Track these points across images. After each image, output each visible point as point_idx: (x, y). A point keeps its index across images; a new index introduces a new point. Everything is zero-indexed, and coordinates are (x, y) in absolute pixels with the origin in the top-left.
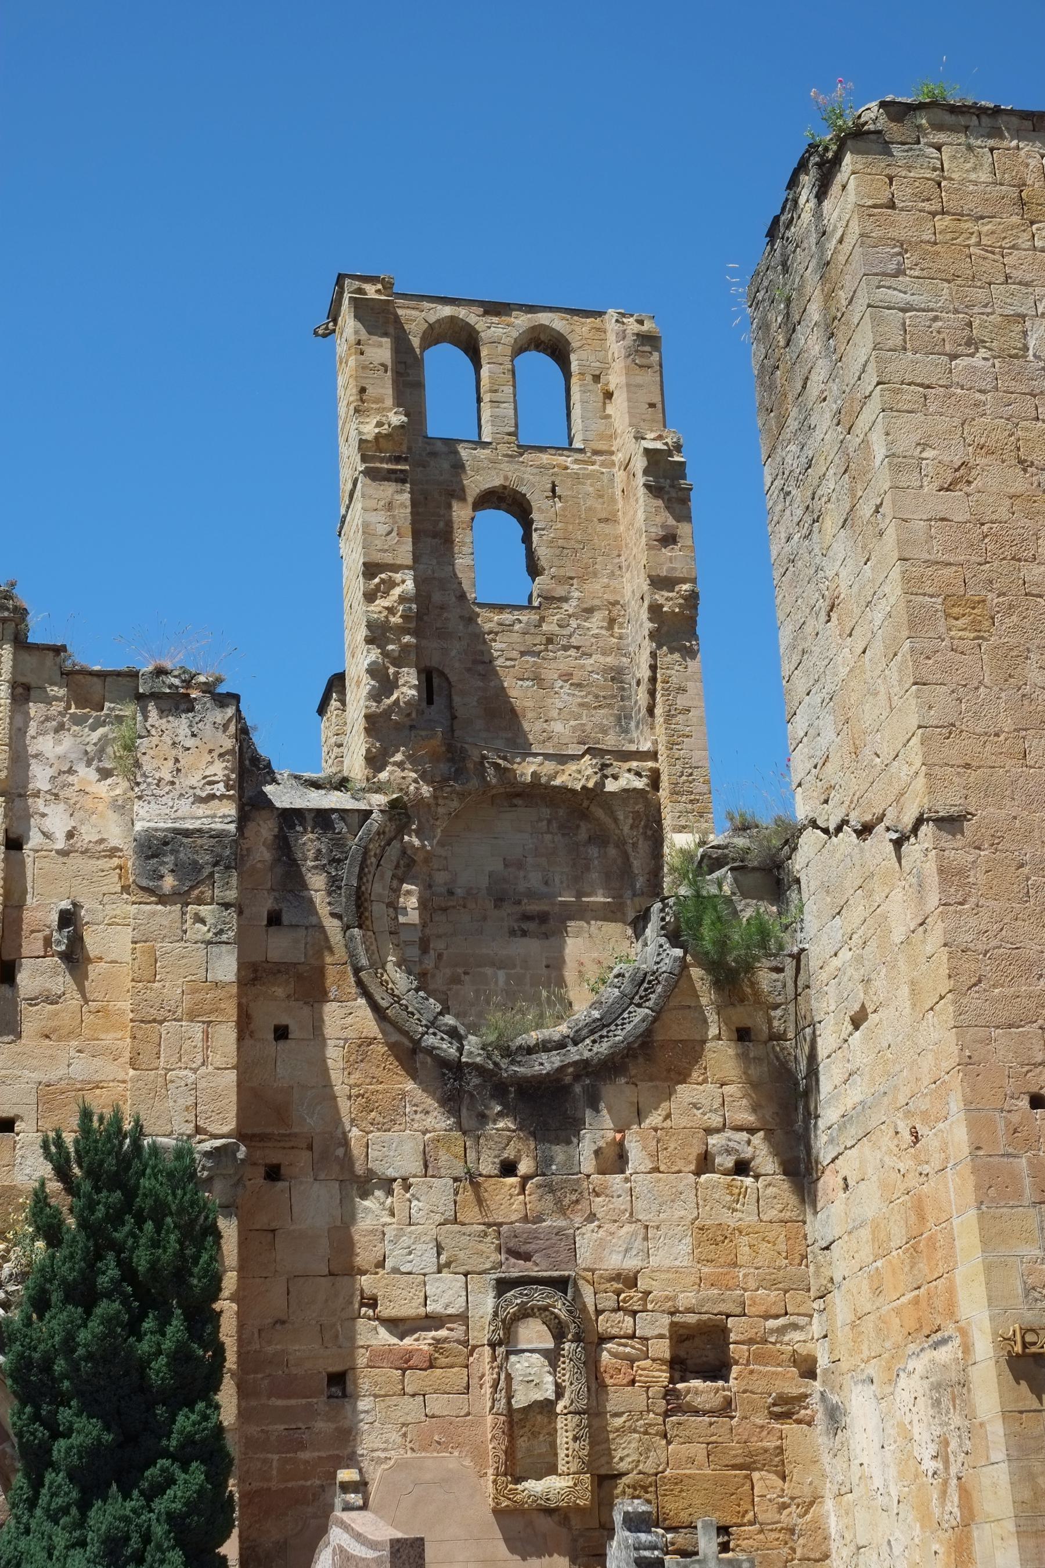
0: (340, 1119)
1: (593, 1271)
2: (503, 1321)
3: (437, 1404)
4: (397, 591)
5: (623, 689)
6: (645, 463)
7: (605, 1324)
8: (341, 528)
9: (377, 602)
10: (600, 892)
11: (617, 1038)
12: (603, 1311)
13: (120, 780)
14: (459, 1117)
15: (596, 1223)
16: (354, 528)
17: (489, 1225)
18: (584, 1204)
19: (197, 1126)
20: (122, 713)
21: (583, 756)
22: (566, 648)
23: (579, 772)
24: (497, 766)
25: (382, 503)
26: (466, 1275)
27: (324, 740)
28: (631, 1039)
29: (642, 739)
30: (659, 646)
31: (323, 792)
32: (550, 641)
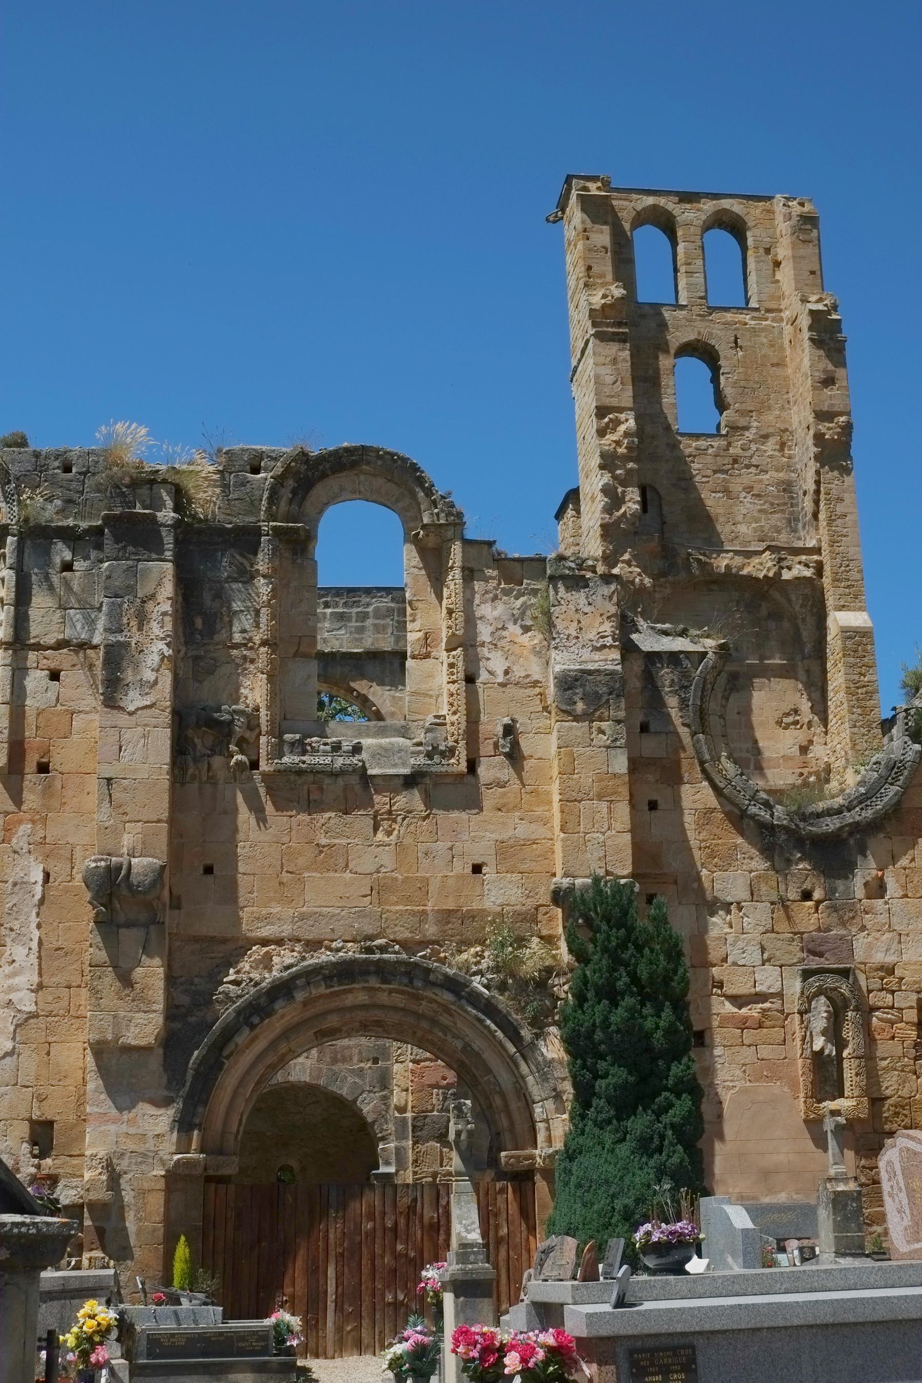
0: (695, 863)
1: (865, 964)
2: (807, 997)
3: (765, 1051)
4: (622, 428)
5: (792, 498)
6: (810, 322)
7: (873, 999)
8: (573, 375)
9: (607, 437)
10: (778, 655)
11: (878, 807)
12: (873, 991)
13: (536, 633)
14: (773, 862)
15: (866, 932)
16: (586, 377)
17: (795, 934)
18: (858, 919)
19: (606, 871)
20: (535, 587)
21: (764, 551)
22: (748, 467)
23: (761, 564)
24: (699, 561)
25: (609, 359)
26: (781, 967)
27: (561, 539)
28: (888, 808)
29: (808, 538)
30: (822, 466)
31: (671, 638)
32: (735, 461)
